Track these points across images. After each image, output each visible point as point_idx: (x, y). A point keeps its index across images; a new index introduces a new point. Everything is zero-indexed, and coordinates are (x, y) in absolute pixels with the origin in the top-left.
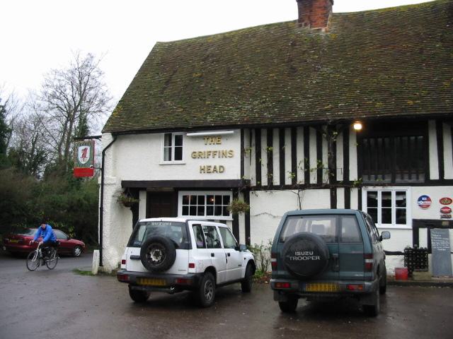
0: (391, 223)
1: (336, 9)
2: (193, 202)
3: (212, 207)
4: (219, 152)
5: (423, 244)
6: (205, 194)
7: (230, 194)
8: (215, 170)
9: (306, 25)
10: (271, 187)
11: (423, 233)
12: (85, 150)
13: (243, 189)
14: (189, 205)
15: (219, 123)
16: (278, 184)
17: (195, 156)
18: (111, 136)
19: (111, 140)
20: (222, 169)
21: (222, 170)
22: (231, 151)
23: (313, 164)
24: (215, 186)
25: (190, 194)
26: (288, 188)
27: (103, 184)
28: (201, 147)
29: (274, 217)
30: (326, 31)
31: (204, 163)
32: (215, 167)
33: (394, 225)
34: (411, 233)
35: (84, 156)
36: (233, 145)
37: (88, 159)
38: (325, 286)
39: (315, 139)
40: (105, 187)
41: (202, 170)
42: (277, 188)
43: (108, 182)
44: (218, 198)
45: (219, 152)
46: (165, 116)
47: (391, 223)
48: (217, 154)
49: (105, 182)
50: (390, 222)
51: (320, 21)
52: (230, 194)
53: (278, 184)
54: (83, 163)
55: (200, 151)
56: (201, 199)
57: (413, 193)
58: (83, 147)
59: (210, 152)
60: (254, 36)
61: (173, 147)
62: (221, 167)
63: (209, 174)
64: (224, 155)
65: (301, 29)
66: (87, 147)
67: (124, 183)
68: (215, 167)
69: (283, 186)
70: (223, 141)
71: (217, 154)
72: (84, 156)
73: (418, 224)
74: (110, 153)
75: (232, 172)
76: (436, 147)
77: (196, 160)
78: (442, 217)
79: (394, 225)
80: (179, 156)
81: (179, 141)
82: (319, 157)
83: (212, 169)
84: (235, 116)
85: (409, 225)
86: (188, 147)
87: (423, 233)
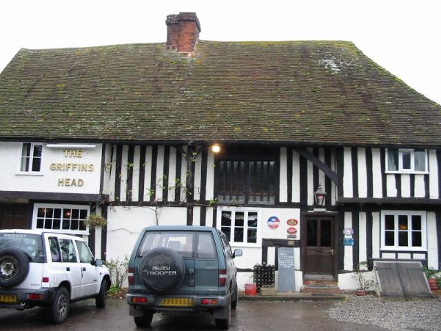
2: (49, 215)
5: (271, 262)
6: (62, 207)
7: (88, 208)
8: (74, 183)
9: (173, 48)
10: (129, 203)
11: (271, 251)
13: (101, 204)
14: (45, 218)
17: (54, 168)
20: (81, 183)
21: (81, 183)
23: (172, 182)
25: (46, 206)
26: (147, 204)
28: (61, 159)
29: (131, 233)
30: (192, 56)
31: (62, 175)
32: (74, 181)
36: (93, 158)
41: (60, 182)
42: (135, 204)
44: (50, 211)
50: (406, 245)
51: (187, 46)
52: (88, 208)
56: (58, 212)
57: (264, 214)
59: (70, 165)
61: (410, 231)
62: (80, 180)
64: (84, 168)
68: (74, 181)
69: (141, 203)
70: (84, 155)
73: (267, 243)
75: (91, 187)
78: (288, 237)
80: (36, 167)
81: (38, 152)
82: (178, 176)
83: (70, 183)
84: (98, 130)
85: (259, 243)
86: (47, 158)
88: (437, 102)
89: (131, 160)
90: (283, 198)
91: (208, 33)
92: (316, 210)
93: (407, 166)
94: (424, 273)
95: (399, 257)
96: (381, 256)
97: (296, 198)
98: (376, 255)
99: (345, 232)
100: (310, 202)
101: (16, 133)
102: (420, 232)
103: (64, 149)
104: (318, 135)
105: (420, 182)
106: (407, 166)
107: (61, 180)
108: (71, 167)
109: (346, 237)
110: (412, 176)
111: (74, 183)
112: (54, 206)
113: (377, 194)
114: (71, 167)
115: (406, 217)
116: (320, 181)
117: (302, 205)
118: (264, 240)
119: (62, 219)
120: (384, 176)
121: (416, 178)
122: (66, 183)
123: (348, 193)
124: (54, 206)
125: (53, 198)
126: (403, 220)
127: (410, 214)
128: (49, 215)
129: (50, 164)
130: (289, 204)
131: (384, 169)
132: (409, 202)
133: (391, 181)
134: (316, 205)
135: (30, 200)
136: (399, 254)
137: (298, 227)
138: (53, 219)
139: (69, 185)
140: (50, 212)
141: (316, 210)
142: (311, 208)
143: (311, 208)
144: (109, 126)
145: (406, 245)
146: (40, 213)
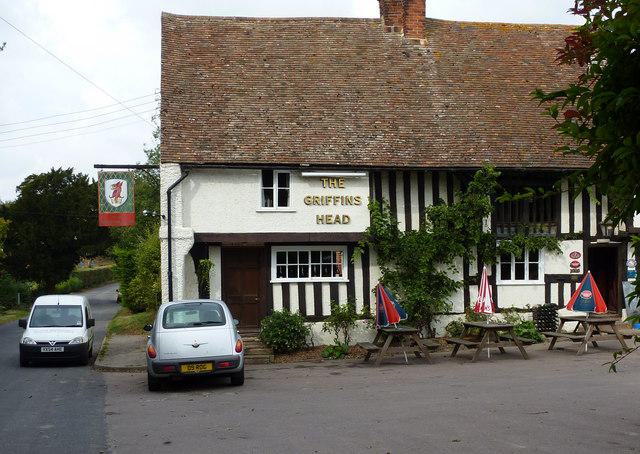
1: (432, 12)
2: (293, 259)
5: (555, 300)
8: (337, 220)
9: (396, 30)
11: (554, 287)
12: (118, 185)
14: (321, 264)
15: (343, 160)
17: (309, 201)
18: (179, 169)
19: (178, 176)
20: (346, 220)
21: (346, 220)
24: (335, 240)
25: (287, 249)
27: (170, 239)
28: (319, 191)
31: (322, 211)
32: (338, 217)
33: (527, 280)
35: (116, 194)
37: (124, 200)
38: (564, 320)
40: (172, 242)
41: (320, 220)
46: (507, 139)
50: (523, 278)
55: (316, 195)
56: (304, 257)
60: (189, 30)
61: (275, 188)
62: (344, 217)
64: (348, 201)
65: (391, 34)
67: (197, 236)
68: (338, 217)
72: (116, 194)
73: (550, 279)
74: (178, 196)
76: (567, 206)
77: (313, 207)
78: (572, 271)
79: (527, 280)
80: (284, 200)
81: (284, 181)
83: (333, 219)
85: (541, 280)
86: (298, 190)
87: (554, 287)
90: (565, 229)
92: (599, 241)
94: (41, 301)
97: (579, 228)
99: (628, 264)
100: (593, 232)
101: (248, 158)
103: (320, 179)
107: (320, 217)
109: (629, 269)
112: (298, 249)
115: (307, 253)
116: (399, 217)
117: (584, 235)
119: (310, 264)
124: (298, 249)
125: (312, 240)
128: (293, 259)
130: (572, 236)
134: (600, 235)
135: (266, 244)
137: (581, 260)
138: (287, 265)
140: (293, 257)
141: (599, 241)
142: (594, 239)
143: (594, 239)
144: (371, 151)
145: (523, 278)
146: (281, 258)
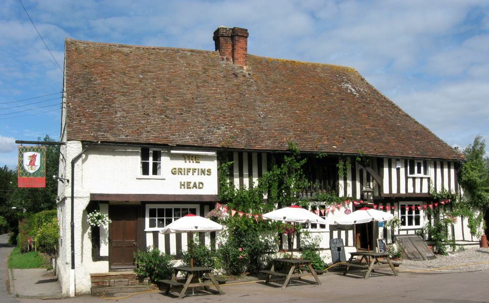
0: (150, 227)
3: (158, 217)
4: (198, 169)
8: (195, 186)
9: (227, 59)
11: (335, 233)
12: (34, 157)
15: (200, 143)
16: (351, 196)
18: (80, 145)
21: (201, 186)
22: (210, 170)
27: (72, 198)
28: (181, 164)
32: (195, 183)
34: (328, 234)
35: (32, 163)
37: (37, 168)
39: (257, 167)
41: (182, 185)
43: (78, 196)
45: (184, 169)
47: (150, 227)
48: (197, 171)
49: (75, 195)
53: (351, 196)
54: (31, 172)
58: (31, 153)
59: (190, 169)
63: (189, 190)
64: (203, 172)
66: (36, 153)
68: (195, 183)
71: (197, 171)
72: (32, 163)
81: (157, 156)
83: (192, 185)
88: (278, 58)
89: (345, 179)
91: (255, 47)
93: (419, 172)
95: (409, 233)
96: (399, 233)
98: (396, 233)
102: (158, 209)
104: (370, 150)
105: (425, 182)
106: (419, 172)
107: (183, 183)
108: (191, 171)
110: (414, 179)
111: (195, 186)
113: (403, 191)
114: (191, 171)
118: (331, 226)
120: (407, 178)
121: (423, 180)
122: (188, 185)
123: (386, 191)
126: (410, 206)
127: (414, 203)
129: (212, 174)
131: (407, 173)
132: (419, 196)
133: (410, 181)
136: (409, 231)
139: (190, 188)
144: (220, 136)
